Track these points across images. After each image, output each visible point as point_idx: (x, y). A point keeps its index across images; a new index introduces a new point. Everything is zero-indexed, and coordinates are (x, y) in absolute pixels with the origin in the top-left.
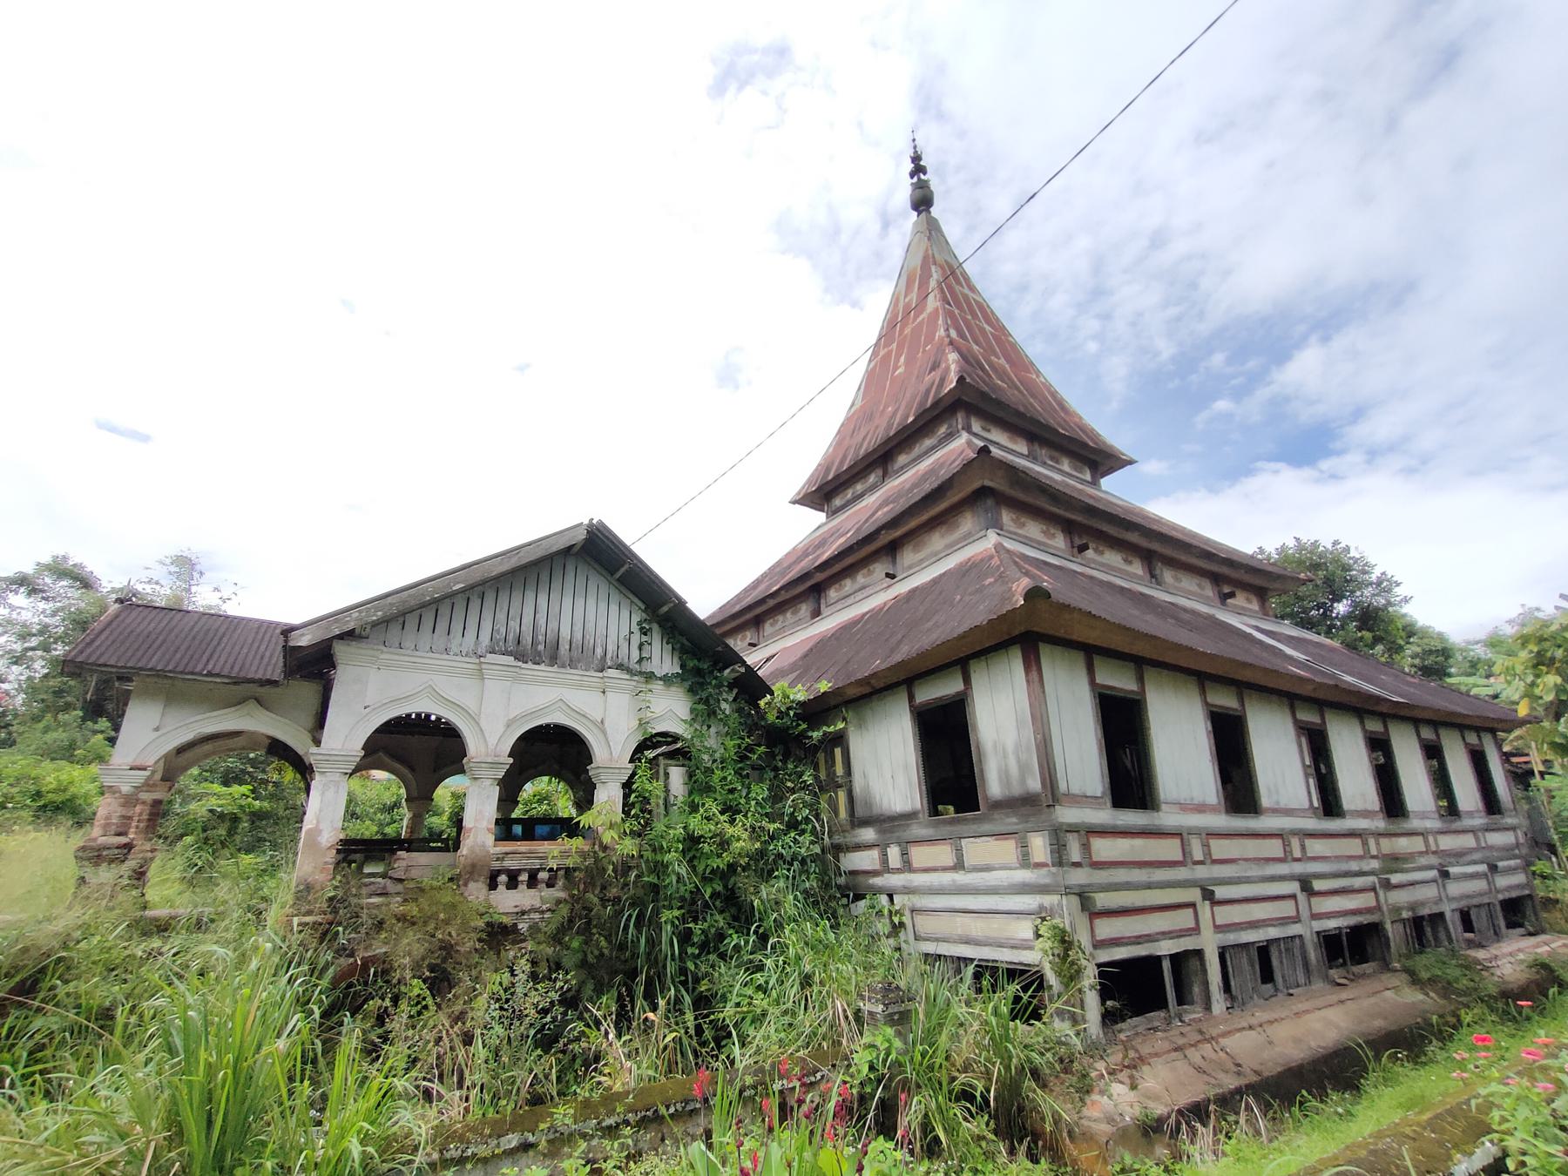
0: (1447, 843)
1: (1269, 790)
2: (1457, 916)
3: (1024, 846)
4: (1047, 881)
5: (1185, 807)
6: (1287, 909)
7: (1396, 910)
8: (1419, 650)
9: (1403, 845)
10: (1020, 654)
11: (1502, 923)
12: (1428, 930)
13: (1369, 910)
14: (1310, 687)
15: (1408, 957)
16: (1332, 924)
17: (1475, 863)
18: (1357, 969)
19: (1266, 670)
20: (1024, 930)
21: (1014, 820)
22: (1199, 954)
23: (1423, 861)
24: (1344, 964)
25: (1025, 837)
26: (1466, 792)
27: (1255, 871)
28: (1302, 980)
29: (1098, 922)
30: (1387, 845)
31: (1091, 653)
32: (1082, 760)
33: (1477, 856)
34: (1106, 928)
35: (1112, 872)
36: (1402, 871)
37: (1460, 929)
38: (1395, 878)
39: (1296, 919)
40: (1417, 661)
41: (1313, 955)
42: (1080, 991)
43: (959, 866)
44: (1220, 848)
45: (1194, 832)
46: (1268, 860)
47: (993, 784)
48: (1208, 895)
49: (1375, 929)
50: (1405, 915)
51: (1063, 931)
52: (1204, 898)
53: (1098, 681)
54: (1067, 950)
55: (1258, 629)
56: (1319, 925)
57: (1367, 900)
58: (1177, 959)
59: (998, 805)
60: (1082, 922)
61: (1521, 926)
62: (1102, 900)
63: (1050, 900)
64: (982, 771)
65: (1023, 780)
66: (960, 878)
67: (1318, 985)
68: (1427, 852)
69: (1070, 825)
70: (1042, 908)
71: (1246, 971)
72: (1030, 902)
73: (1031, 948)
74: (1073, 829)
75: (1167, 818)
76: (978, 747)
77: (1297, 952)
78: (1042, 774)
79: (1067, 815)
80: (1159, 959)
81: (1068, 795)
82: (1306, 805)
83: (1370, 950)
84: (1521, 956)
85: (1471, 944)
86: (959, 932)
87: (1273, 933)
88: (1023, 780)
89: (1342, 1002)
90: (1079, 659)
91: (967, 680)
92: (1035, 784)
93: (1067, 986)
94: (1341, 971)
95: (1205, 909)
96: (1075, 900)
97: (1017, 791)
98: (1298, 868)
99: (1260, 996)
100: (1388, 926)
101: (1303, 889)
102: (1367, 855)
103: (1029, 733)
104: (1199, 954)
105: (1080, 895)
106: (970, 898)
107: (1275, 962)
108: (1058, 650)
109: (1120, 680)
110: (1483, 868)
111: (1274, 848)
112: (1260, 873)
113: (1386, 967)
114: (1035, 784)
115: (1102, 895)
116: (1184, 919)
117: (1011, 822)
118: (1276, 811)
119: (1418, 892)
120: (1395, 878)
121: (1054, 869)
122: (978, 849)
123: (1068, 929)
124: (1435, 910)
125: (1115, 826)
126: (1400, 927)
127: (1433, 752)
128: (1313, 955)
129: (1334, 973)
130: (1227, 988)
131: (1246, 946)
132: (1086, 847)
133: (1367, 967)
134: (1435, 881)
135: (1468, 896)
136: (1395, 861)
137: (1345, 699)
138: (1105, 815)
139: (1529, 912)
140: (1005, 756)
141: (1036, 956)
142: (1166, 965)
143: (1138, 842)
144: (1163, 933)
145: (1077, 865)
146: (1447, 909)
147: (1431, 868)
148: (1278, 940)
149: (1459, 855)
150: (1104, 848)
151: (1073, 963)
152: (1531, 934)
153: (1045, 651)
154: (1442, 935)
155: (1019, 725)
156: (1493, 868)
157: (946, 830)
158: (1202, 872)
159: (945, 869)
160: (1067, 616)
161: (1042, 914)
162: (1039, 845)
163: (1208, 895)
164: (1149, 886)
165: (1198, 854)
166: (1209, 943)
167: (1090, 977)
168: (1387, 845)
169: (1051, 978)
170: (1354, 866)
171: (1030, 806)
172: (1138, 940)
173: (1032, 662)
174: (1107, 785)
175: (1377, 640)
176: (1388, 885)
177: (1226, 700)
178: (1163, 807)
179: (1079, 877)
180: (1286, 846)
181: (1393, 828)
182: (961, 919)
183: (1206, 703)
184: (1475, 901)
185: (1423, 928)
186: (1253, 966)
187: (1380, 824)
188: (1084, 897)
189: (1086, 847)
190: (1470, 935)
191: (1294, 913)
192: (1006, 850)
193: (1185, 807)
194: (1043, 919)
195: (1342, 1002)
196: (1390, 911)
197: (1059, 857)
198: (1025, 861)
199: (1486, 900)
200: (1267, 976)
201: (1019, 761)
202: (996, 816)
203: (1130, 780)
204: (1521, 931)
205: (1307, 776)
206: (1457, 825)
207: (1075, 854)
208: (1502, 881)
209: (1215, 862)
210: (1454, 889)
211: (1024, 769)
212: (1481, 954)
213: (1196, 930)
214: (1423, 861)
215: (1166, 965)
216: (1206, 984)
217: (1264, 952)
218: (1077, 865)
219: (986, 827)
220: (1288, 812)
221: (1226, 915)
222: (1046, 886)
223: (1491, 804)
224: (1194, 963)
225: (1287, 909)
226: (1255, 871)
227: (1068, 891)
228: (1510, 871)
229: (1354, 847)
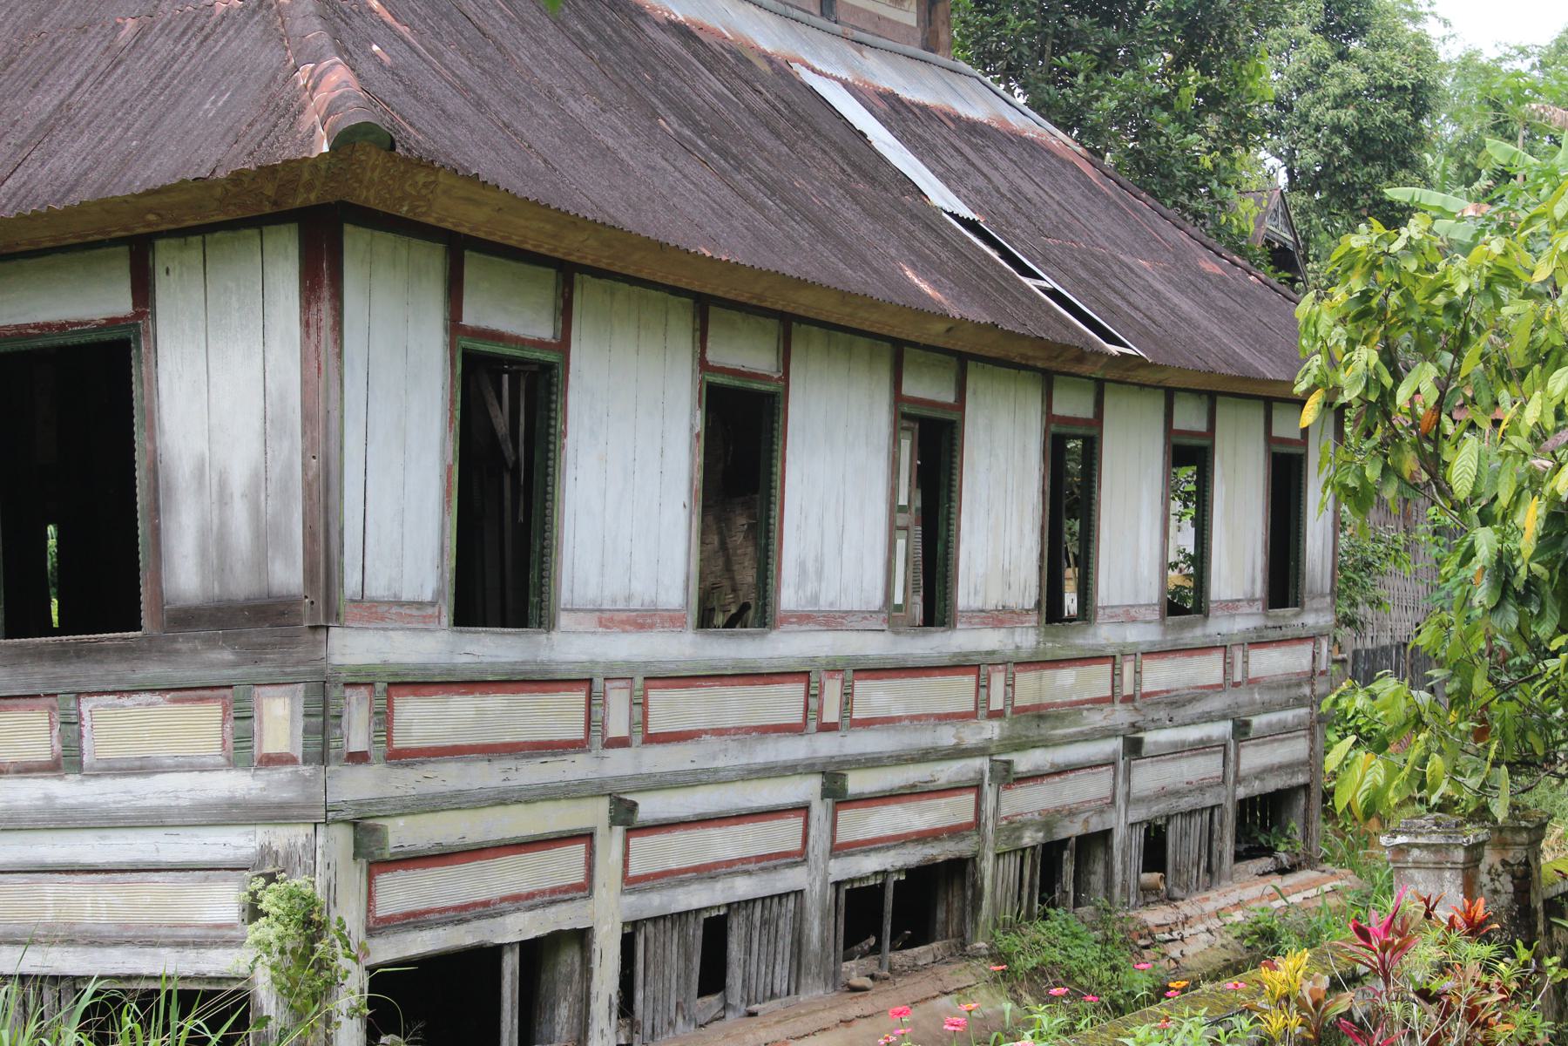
0: (1161, 676)
1: (802, 566)
2: (1138, 836)
3: (243, 717)
4: (287, 795)
5: (612, 619)
6: (786, 834)
7: (1014, 827)
8: (1359, 80)
9: (1066, 683)
10: (293, 251)
11: (1228, 847)
12: (1068, 869)
13: (955, 832)
14: (940, 327)
15: (1010, 928)
16: (867, 865)
17: (1209, 718)
18: (898, 958)
19: (845, 296)
20: (220, 903)
21: (228, 655)
22: (581, 938)
23: (1096, 719)
24: (876, 950)
25: (248, 698)
26: (1237, 563)
27: (732, 756)
28: (781, 985)
29: (384, 880)
30: (1030, 688)
31: (458, 252)
32: (403, 522)
33: (1216, 703)
34: (398, 893)
35: (430, 769)
36: (1045, 743)
37: (1136, 859)
38: (1025, 762)
39: (799, 857)
40: (1348, 116)
41: (815, 930)
42: (328, 1019)
43: (67, 762)
44: (668, 710)
45: (619, 674)
46: (765, 730)
47: (183, 565)
48: (623, 813)
49: (958, 871)
50: (1030, 838)
51: (310, 902)
52: (614, 821)
53: (469, 319)
54: (312, 940)
55: (894, 110)
56: (843, 869)
57: (958, 810)
58: (535, 953)
59: (187, 619)
60: (352, 878)
61: (1269, 851)
62: (402, 833)
63: (283, 837)
64: (156, 531)
65: (260, 565)
66: (68, 791)
67: (814, 992)
68: (1110, 700)
69: (356, 670)
70: (266, 853)
71: (674, 964)
72: (239, 843)
73: (229, 943)
74: (360, 680)
75: (569, 644)
76: (154, 471)
77: (785, 927)
78: (309, 553)
79: (352, 647)
80: (496, 951)
81: (361, 601)
82: (877, 600)
83: (941, 915)
84: (1238, 916)
85: (1149, 895)
86: (49, 917)
87: (743, 888)
88: (260, 565)
89: (846, 1022)
90: (433, 259)
91: (143, 292)
92: (288, 575)
93: (299, 1016)
94: (870, 964)
95: (610, 845)
96: (342, 837)
97: (242, 586)
98: (826, 746)
99: (689, 1019)
100: (987, 866)
101: (826, 793)
102: (981, 711)
103: (290, 450)
104: (581, 938)
105: (355, 824)
106: (157, 835)
107: (735, 950)
108: (385, 242)
109: (511, 313)
110: (1222, 729)
111: (785, 702)
112: (743, 760)
113: (961, 951)
114: (288, 575)
115: (401, 822)
116: (565, 865)
117: (219, 660)
118: (803, 618)
119: (1071, 791)
120: (1025, 762)
121: (307, 770)
122: (114, 725)
123: (320, 896)
124: (1096, 825)
125: (451, 669)
126: (1012, 863)
127: (1190, 455)
128: (815, 930)
129: (854, 971)
130: (626, 1007)
131: (680, 917)
132: (384, 720)
133: (923, 953)
134: (1111, 763)
135: (1177, 794)
136: (1038, 720)
137: (1014, 352)
138: (437, 646)
139: (1295, 825)
140: (223, 499)
141: (249, 961)
142: (511, 964)
143: (495, 702)
144: (516, 898)
145: (359, 758)
146: (1118, 822)
147: (1107, 734)
148: (748, 903)
149: (1175, 703)
150: (420, 720)
151: (321, 965)
152: (1282, 871)
153: (355, 242)
154: (1097, 880)
155: (269, 424)
156: (1242, 730)
157: (37, 675)
158: (619, 764)
159: (26, 770)
160: (421, 178)
161: (268, 868)
162: (280, 719)
163: (623, 813)
164: (502, 799)
165: (618, 725)
166: (606, 916)
167: (352, 992)
168: (1030, 688)
169: (267, 999)
170: (946, 736)
171: (272, 625)
172: (461, 914)
173: (321, 277)
174: (450, 575)
175: (1212, 100)
176: (1008, 777)
177: (746, 354)
178: (564, 620)
179: (355, 786)
180: (812, 694)
181: (1054, 648)
182: (51, 889)
183: (703, 365)
184: (1185, 804)
185: (1061, 866)
186: (688, 959)
187: (1027, 639)
188: (363, 830)
189: (384, 720)
190: (1152, 878)
191: (796, 845)
192: (201, 725)
193: (612, 619)
194: (271, 878)
195: (846, 1022)
196: (998, 830)
197: (322, 742)
198: (241, 750)
199: (1209, 800)
200: (713, 979)
201: (256, 513)
202: (181, 645)
203: (501, 556)
204: (1266, 863)
205: (893, 529)
206: (1195, 634)
207: (358, 735)
208: (1253, 758)
209: (652, 739)
210: (1147, 777)
211: (264, 537)
212: (1155, 916)
213: (585, 888)
214: (1096, 719)
215: (511, 964)
216: (585, 1000)
217: (716, 929)
218: (359, 758)
219: (153, 671)
220: (832, 620)
221: (651, 853)
222: (281, 806)
223: (1283, 579)
224: (569, 959)
225: (786, 834)
226: (732, 756)
227: (329, 817)
228: (1282, 732)
229: (957, 692)
